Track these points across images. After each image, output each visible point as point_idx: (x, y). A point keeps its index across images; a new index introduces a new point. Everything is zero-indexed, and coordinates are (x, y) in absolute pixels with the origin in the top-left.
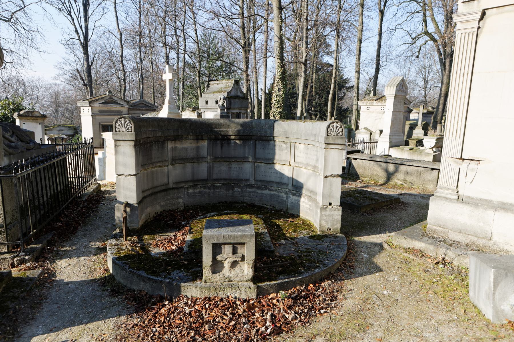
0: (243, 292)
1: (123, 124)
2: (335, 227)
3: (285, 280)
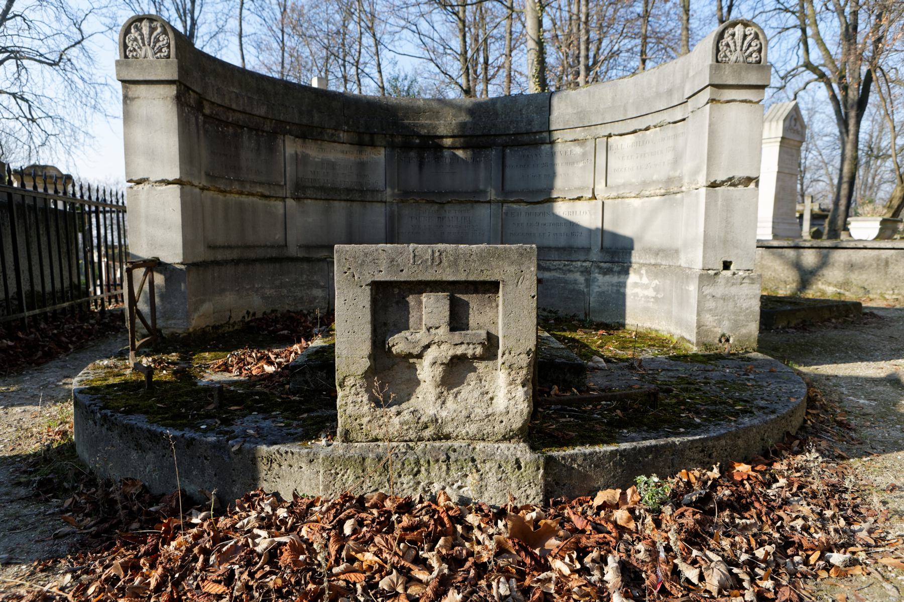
1: (146, 36)
2: (744, 331)
3: (647, 443)
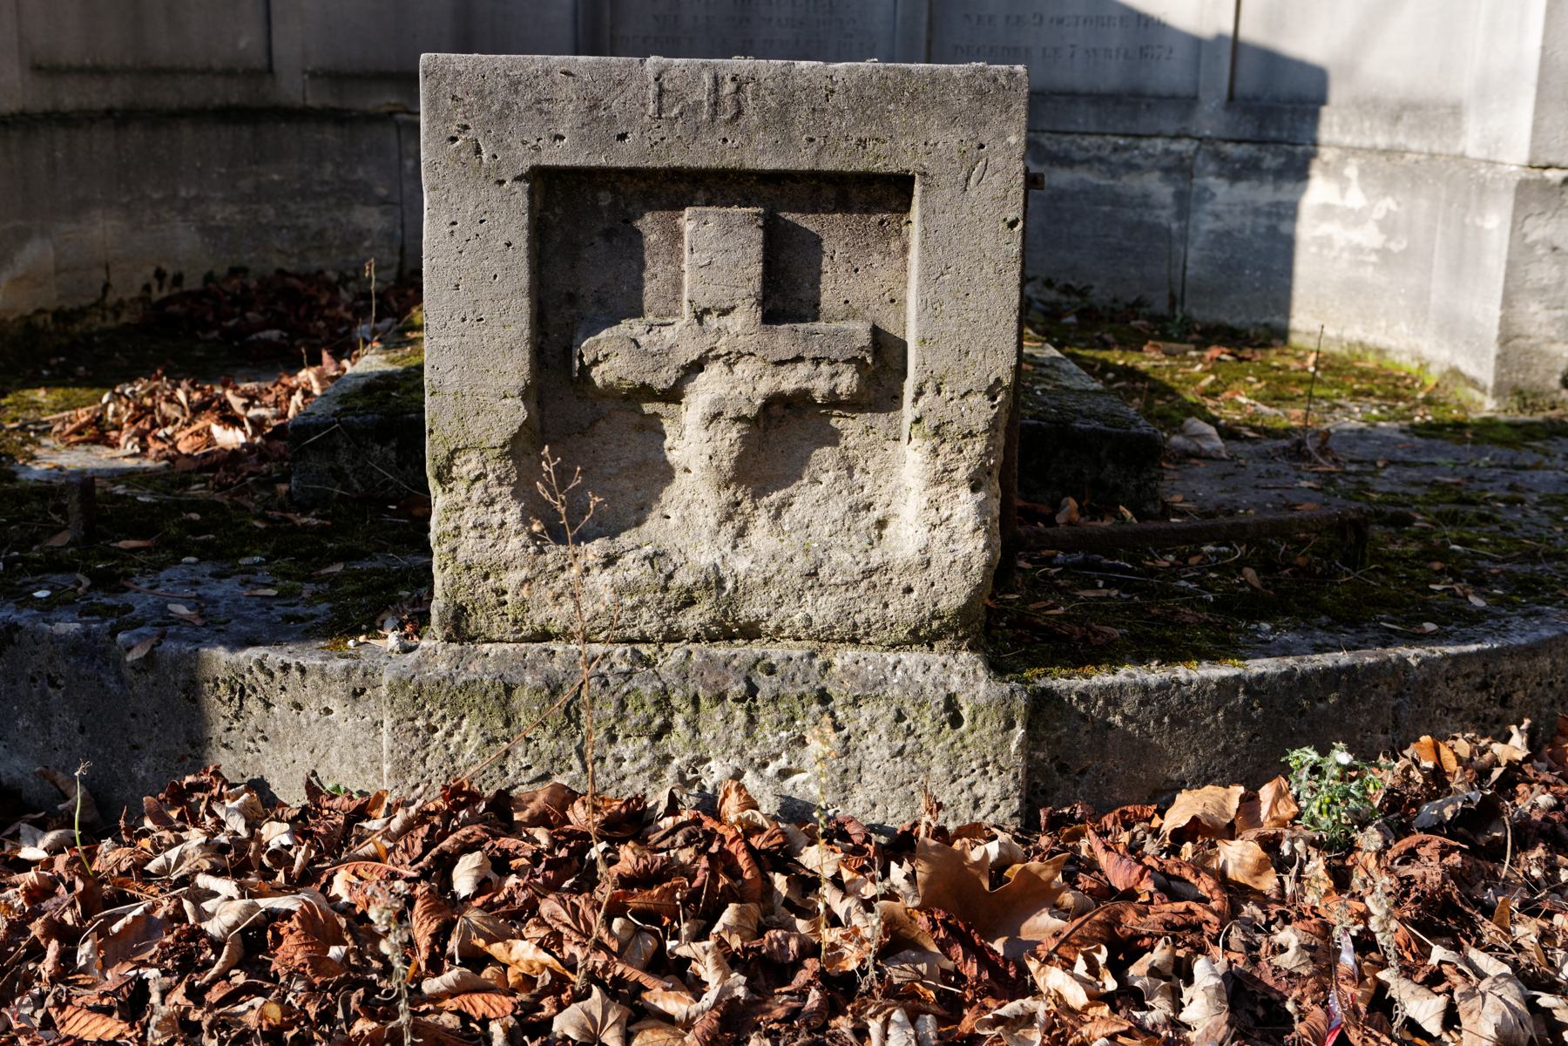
0: (876, 750)
3: (1326, 660)
